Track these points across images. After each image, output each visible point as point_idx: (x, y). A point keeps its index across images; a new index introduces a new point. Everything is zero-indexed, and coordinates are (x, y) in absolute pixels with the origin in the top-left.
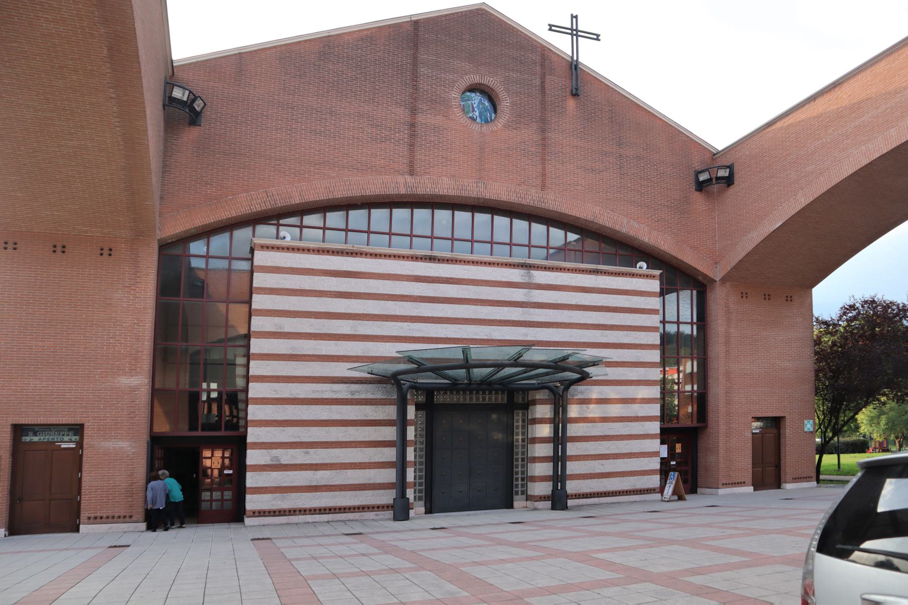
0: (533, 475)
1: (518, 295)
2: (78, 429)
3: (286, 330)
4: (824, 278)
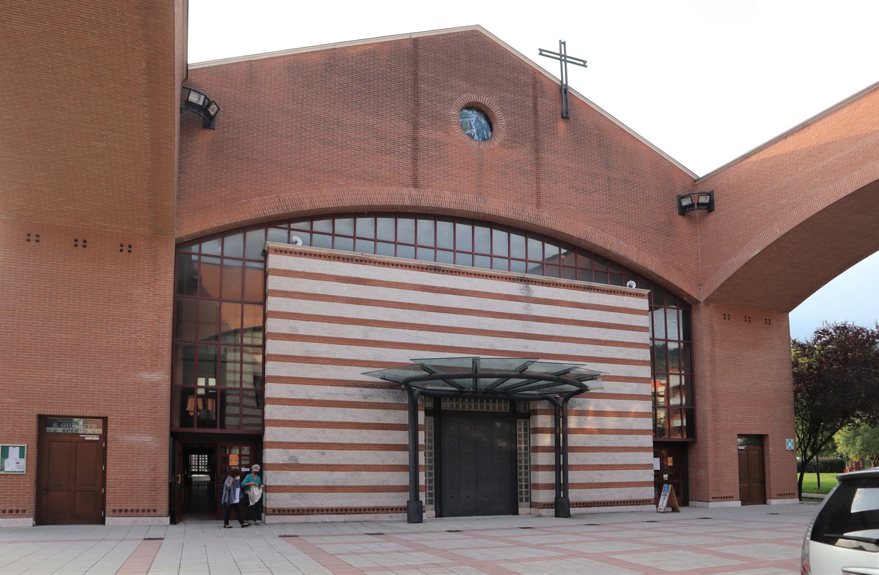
1: (517, 308)
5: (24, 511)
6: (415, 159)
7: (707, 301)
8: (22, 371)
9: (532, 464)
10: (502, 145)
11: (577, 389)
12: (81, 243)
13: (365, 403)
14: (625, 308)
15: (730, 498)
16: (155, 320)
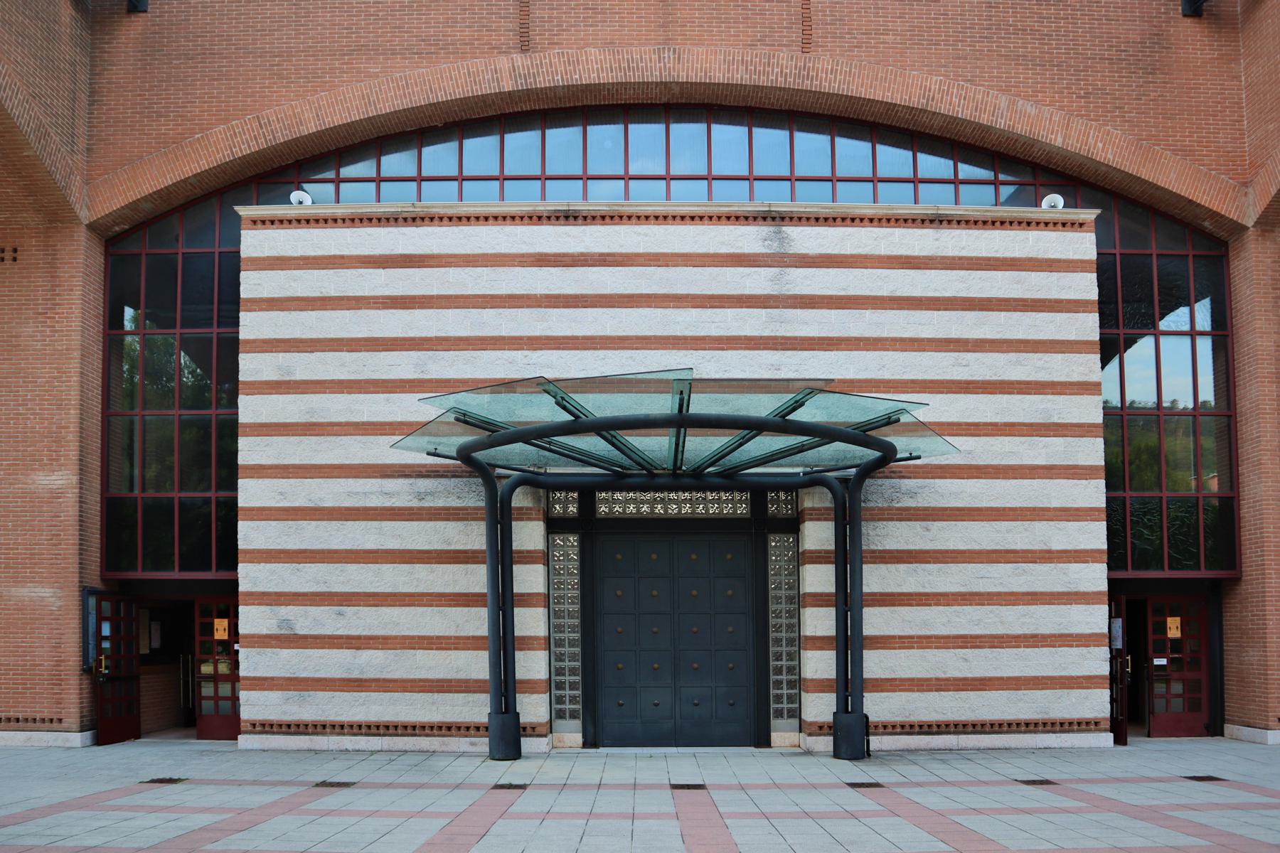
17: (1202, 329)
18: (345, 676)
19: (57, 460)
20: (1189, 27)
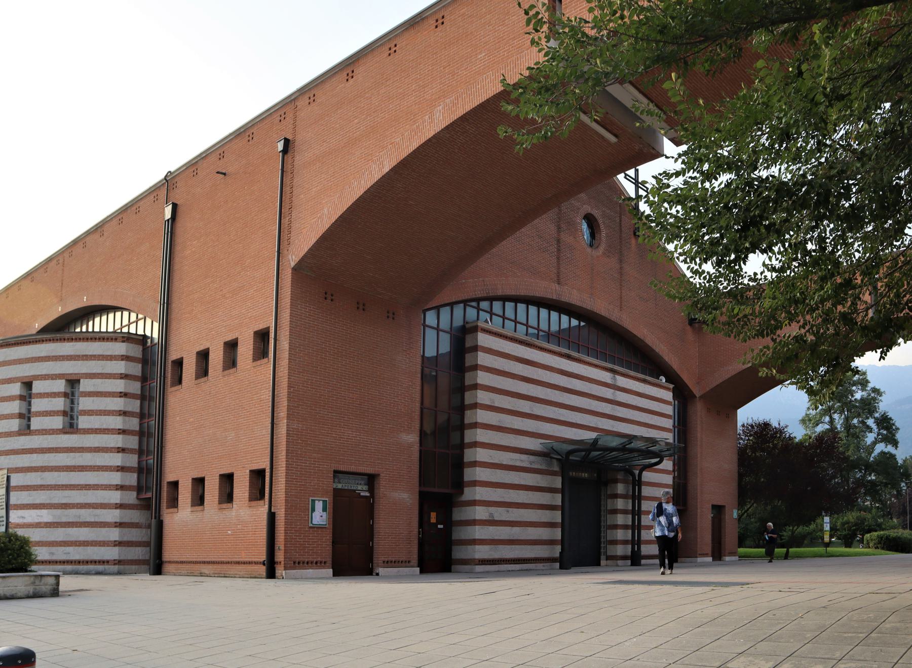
0: (615, 539)
1: (608, 393)
2: (371, 480)
3: (496, 405)
4: (746, 404)
5: (325, 562)
6: (558, 258)
7: (701, 397)
8: (323, 427)
9: (608, 524)
10: (604, 254)
11: (658, 459)
12: (361, 306)
13: (531, 468)
14: (661, 399)
15: (706, 555)
16: (410, 385)
17: (642, 490)
18: (508, 538)
19: (411, 428)
20: (689, 327)
